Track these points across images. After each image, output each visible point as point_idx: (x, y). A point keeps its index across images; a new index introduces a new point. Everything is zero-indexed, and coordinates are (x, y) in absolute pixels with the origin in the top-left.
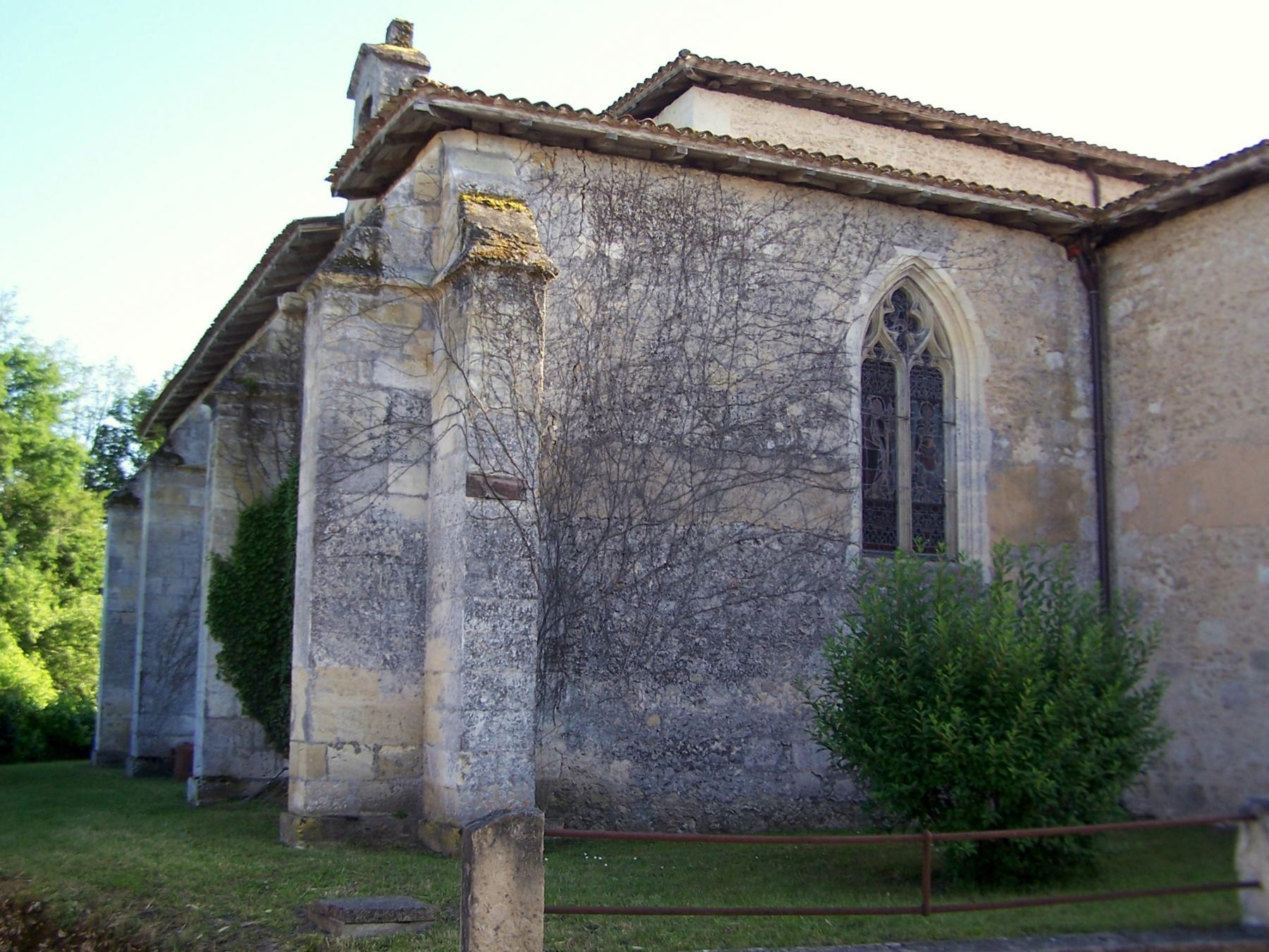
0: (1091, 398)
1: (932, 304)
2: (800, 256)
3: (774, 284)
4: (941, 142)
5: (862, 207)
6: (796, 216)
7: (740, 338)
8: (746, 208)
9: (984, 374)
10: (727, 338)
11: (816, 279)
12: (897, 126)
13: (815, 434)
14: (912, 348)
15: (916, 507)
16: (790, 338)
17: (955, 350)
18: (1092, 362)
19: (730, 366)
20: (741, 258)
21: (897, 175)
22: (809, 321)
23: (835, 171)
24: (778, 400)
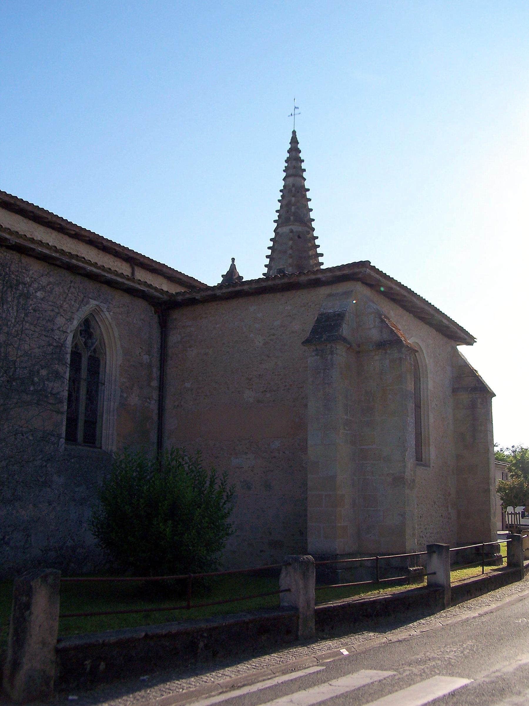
0: (159, 377)
1: (100, 327)
2: (51, 299)
3: (39, 310)
4: (71, 239)
5: (78, 279)
6: (51, 280)
7: (24, 335)
8: (31, 272)
9: (119, 363)
10: (18, 334)
11: (57, 310)
12: (54, 228)
13: (51, 385)
14: (90, 347)
15: (86, 422)
16: (44, 338)
17: (107, 350)
18: (161, 360)
19: (18, 349)
20: (27, 296)
21: (99, 268)
22: (52, 330)
23: (74, 261)
24: (37, 367)
